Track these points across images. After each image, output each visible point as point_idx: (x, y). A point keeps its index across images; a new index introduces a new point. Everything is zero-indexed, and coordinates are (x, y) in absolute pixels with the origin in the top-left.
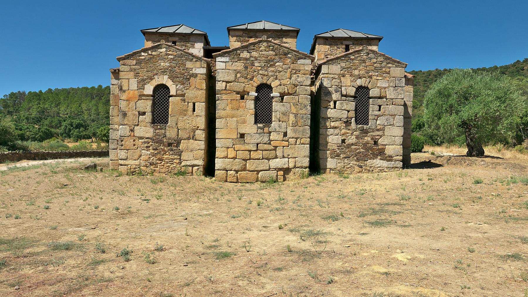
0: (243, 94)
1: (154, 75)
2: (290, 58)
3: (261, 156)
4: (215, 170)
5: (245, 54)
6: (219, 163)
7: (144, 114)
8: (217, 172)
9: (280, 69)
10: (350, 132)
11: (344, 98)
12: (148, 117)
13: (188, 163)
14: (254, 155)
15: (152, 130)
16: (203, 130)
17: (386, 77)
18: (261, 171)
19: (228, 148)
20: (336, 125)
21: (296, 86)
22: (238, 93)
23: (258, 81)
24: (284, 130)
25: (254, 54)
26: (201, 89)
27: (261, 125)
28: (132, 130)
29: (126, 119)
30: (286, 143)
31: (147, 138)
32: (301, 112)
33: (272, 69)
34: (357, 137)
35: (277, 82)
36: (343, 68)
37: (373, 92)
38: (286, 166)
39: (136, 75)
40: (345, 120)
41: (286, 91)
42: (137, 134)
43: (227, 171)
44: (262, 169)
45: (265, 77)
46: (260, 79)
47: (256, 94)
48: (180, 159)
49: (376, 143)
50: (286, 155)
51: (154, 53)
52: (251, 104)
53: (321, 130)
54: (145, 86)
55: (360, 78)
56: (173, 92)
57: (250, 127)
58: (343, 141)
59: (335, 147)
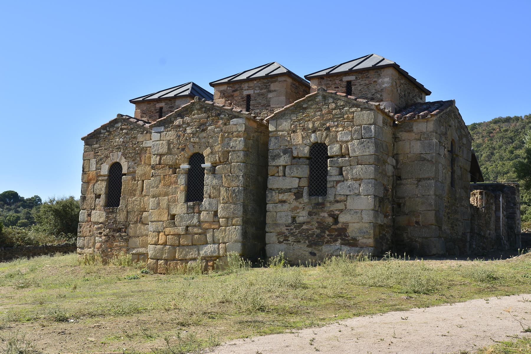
2: (222, 119)
10: (301, 206)
12: (101, 201)
20: (285, 198)
24: (214, 209)
27: (191, 203)
28: (89, 215)
34: (310, 214)
35: (208, 150)
37: (333, 150)
40: (296, 191)
42: (93, 219)
46: (192, 149)
47: (203, 166)
50: (216, 240)
52: (182, 180)
54: (102, 166)
56: (125, 170)
57: (180, 208)
58: (294, 219)
59: (284, 229)
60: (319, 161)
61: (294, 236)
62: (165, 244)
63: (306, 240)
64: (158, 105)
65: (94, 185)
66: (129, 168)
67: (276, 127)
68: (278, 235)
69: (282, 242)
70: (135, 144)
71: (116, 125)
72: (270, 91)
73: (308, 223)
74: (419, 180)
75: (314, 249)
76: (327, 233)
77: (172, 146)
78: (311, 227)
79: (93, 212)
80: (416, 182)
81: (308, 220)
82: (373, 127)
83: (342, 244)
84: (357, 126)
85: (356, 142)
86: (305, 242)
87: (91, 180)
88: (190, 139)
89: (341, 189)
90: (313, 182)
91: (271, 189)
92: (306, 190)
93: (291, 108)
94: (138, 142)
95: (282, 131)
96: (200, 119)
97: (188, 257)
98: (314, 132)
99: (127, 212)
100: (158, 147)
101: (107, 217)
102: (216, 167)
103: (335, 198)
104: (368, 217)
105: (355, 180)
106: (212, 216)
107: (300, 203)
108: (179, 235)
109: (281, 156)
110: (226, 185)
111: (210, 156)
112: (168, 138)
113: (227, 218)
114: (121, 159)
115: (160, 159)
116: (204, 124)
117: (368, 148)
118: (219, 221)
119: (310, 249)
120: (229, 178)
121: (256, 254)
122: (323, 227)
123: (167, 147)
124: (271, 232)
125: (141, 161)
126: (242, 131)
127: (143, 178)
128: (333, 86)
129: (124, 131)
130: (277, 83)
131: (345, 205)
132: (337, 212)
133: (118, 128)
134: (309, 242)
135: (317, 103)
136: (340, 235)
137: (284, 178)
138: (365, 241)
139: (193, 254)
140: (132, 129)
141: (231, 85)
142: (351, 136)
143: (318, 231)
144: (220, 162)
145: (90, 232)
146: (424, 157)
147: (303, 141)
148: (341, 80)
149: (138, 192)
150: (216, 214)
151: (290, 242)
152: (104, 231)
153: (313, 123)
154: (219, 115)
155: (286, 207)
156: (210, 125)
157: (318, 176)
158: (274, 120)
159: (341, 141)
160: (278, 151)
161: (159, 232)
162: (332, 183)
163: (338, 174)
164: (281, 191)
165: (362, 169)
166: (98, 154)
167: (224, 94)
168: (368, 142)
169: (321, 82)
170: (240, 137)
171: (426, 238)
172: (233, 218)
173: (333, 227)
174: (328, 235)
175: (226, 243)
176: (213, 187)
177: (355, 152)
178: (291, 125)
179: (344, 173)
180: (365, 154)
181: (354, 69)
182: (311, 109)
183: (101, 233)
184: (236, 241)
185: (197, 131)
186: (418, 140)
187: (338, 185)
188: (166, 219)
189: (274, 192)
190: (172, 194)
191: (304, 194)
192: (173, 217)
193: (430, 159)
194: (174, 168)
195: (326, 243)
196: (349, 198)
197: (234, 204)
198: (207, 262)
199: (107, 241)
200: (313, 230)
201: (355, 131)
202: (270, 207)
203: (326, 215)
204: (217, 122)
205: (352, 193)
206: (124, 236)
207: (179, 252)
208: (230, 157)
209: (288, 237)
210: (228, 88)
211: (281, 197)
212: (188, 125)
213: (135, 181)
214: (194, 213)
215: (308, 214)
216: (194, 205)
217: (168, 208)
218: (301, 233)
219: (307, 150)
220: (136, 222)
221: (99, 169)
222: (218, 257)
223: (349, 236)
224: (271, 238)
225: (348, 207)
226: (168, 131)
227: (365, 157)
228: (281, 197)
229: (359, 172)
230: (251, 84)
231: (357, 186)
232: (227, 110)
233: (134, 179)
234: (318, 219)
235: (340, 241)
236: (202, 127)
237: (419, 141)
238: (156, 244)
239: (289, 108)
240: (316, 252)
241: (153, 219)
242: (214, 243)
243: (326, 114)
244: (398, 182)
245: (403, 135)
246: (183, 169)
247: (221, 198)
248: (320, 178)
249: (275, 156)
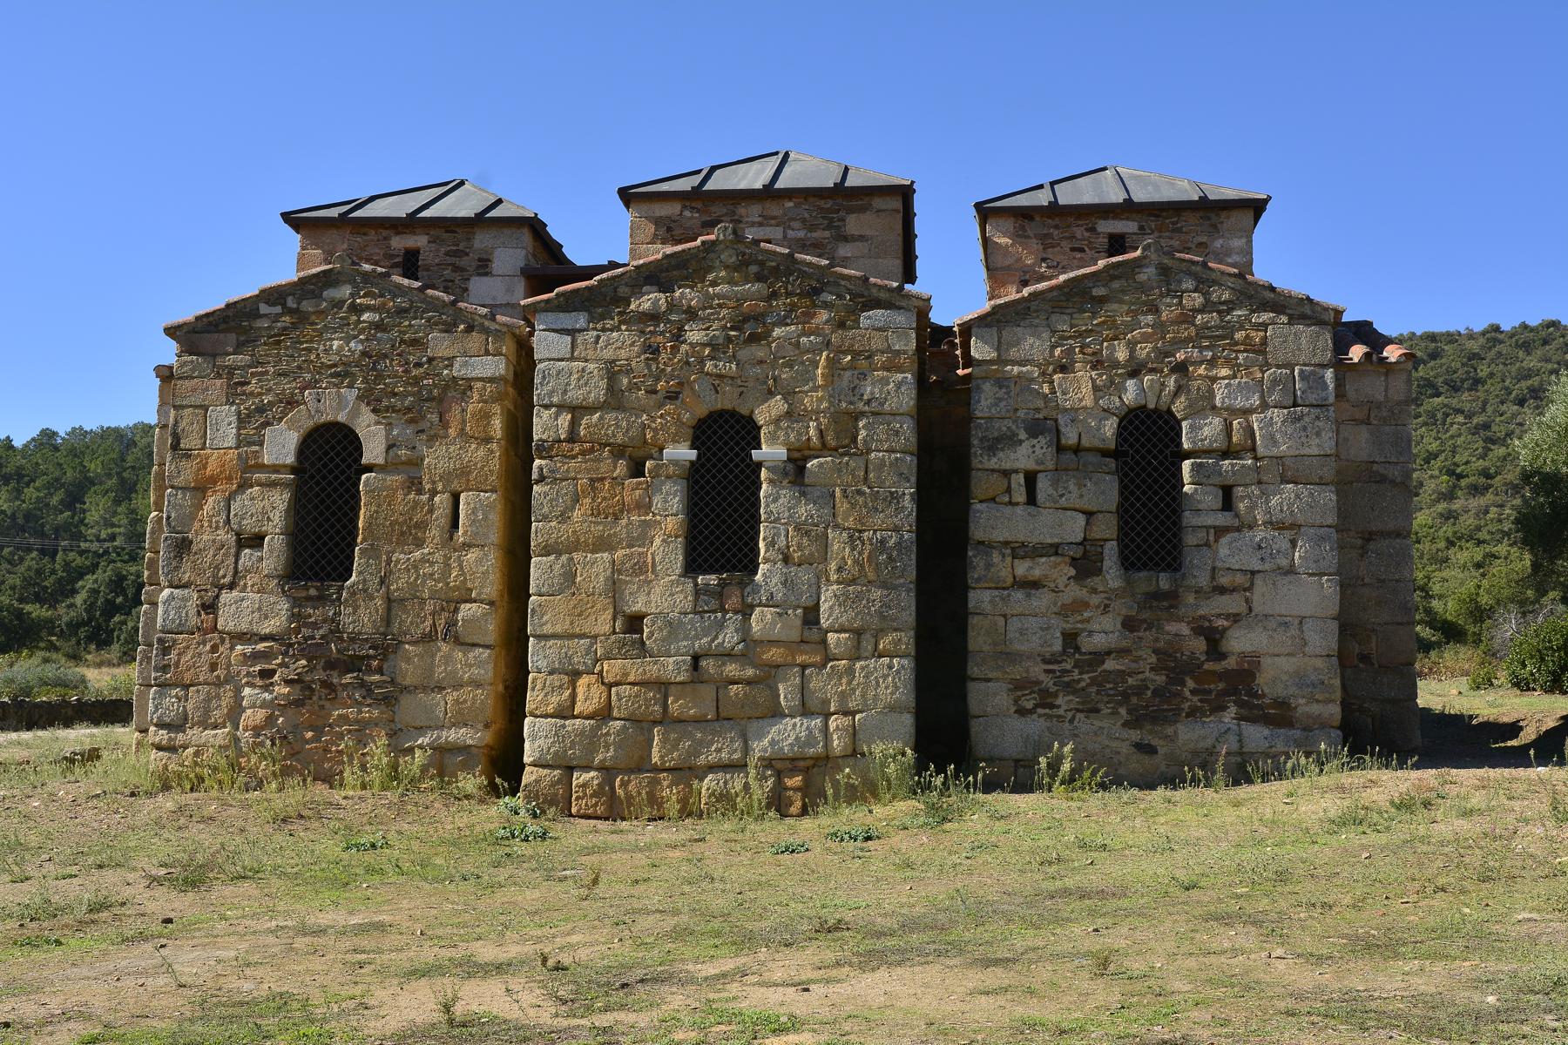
0: (640, 453)
1: (303, 389)
2: (827, 306)
4: (523, 766)
6: (537, 737)
7: (257, 541)
8: (529, 775)
10: (1095, 600)
12: (272, 556)
16: (986, 546)
20: (1037, 573)
22: (619, 452)
24: (805, 600)
27: (713, 579)
28: (210, 607)
29: (186, 565)
34: (1129, 624)
35: (777, 405)
37: (1198, 432)
39: (234, 392)
40: (1079, 552)
43: (570, 769)
47: (692, 454)
50: (813, 704)
52: (669, 505)
53: (971, 594)
56: (373, 452)
57: (665, 593)
58: (1070, 639)
59: (1037, 671)
60: (1150, 463)
61: (1075, 692)
62: (604, 714)
63: (1120, 704)
64: (399, 243)
65: (228, 501)
66: (389, 447)
67: (998, 349)
68: (1017, 688)
69: (1031, 712)
70: (418, 365)
71: (329, 293)
72: (846, 239)
73: (1122, 652)
74: (1369, 537)
75: (1151, 732)
76: (1191, 684)
77: (625, 381)
78: (1134, 665)
79: (226, 597)
80: (1359, 542)
81: (1124, 644)
82: (1329, 374)
83: (1240, 718)
84: (1278, 367)
85: (1277, 415)
86: (1115, 713)
87: (213, 480)
88: (702, 362)
90: (1132, 529)
92: (1111, 551)
93: (1050, 295)
94: (430, 360)
95: (1021, 363)
96: (740, 300)
97: (701, 760)
98: (1134, 373)
99: (389, 600)
100: (563, 380)
101: (293, 617)
102: (806, 459)
103: (1213, 578)
105: (1279, 526)
106: (798, 622)
107: (1094, 591)
108: (662, 686)
109: (1021, 442)
110: (850, 523)
111: (784, 424)
112: (608, 354)
113: (858, 633)
114: (355, 413)
115: (574, 424)
116: (758, 318)
117: (1318, 434)
118: (824, 642)
119: (1135, 735)
120: (861, 500)
121: (948, 744)
122: (1174, 665)
123: (603, 384)
124: (989, 680)
125: (445, 424)
126: (905, 352)
127: (455, 486)
128: (1064, 243)
129: (365, 317)
130: (868, 217)
131: (1247, 600)
132: (1221, 623)
133: (339, 304)
134: (1129, 712)
135: (1143, 288)
136: (1231, 691)
137: (1031, 509)
138: (1315, 709)
139: (723, 748)
140: (401, 312)
141: (699, 205)
142: (1262, 397)
143: (1160, 679)
144: (824, 445)
145: (213, 667)
146: (1382, 471)
147: (1096, 400)
148: (1093, 230)
149: (434, 533)
150: (811, 616)
151: (1061, 712)
152: (283, 665)
153: (1132, 346)
154: (816, 292)
155: (1041, 600)
156: (782, 323)
157: (1150, 511)
158: (989, 326)
159: (1226, 409)
161: (575, 675)
162: (1202, 534)
163: (1220, 505)
164: (1019, 551)
165: (1297, 496)
166: (248, 388)
167: (669, 229)
168: (1318, 418)
169: (1023, 228)
170: (900, 370)
172: (878, 634)
173: (1208, 666)
174: (1193, 692)
175: (853, 714)
176: (797, 529)
177: (1275, 443)
178: (1053, 347)
179: (1241, 507)
180: (1307, 451)
181: (424, 214)
182: (1121, 302)
183: (267, 674)
184: (892, 708)
185: (729, 339)
186: (1362, 422)
188: (607, 628)
190: (630, 546)
191: (1107, 563)
192: (634, 623)
193: (1399, 480)
195: (1188, 716)
196: (1258, 581)
197: (884, 585)
198: (779, 775)
199: (298, 703)
200: (1141, 676)
201: (1275, 382)
202: (980, 598)
203: (1185, 630)
204: (809, 316)
205: (1267, 566)
206: (379, 685)
207: (664, 741)
208: (862, 434)
209: (1055, 695)
210: (687, 213)
211: (1022, 568)
212: (692, 314)
213: (420, 492)
214: (725, 612)
215: (1124, 625)
216: (723, 584)
217: (614, 589)
218: (1100, 685)
219: (1110, 427)
220: (428, 638)
221: (254, 443)
223: (1264, 695)
225: (1257, 608)
226: (604, 330)
227: (1307, 461)
228: (1022, 568)
229: (1290, 505)
230: (774, 209)
231: (1286, 545)
232: (848, 278)
233: (414, 484)
234: (1157, 640)
235: (1233, 709)
236: (750, 327)
237: (1364, 427)
238: (565, 712)
239: (1042, 292)
240: (1154, 742)
241: (547, 629)
242: (805, 711)
243: (1173, 323)
246: (675, 463)
247: (833, 566)
248: (1156, 517)
249: (998, 440)
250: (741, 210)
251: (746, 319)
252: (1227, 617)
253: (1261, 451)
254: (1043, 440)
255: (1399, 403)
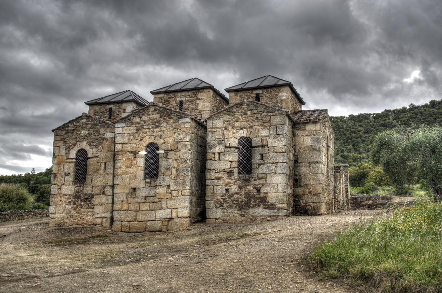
2: (173, 118)
3: (148, 208)
5: (137, 120)
9: (165, 129)
11: (228, 149)
12: (71, 178)
13: (99, 216)
14: (143, 207)
15: (73, 188)
17: (266, 126)
18: (149, 221)
19: (123, 201)
20: (220, 176)
21: (178, 143)
22: (131, 152)
23: (147, 140)
25: (144, 118)
26: (111, 151)
27: (148, 180)
28: (60, 189)
30: (169, 195)
31: (69, 195)
32: (181, 166)
33: (158, 130)
34: (240, 187)
35: (162, 141)
36: (225, 121)
38: (169, 217)
39: (65, 143)
41: (170, 149)
42: (63, 192)
44: (149, 219)
45: (152, 137)
46: (148, 139)
47: (158, 152)
48: (93, 212)
49: (259, 191)
51: (78, 124)
52: (141, 162)
55: (241, 129)
56: (90, 155)
57: (140, 182)
58: (227, 190)
59: (219, 198)
64: (108, 107)
69: (218, 207)
72: (198, 99)
73: (238, 193)
80: (309, 165)
86: (236, 207)
89: (263, 170)
91: (209, 169)
92: (236, 170)
94: (100, 134)
104: (281, 189)
116: (158, 122)
119: (240, 212)
131: (266, 181)
132: (259, 186)
136: (262, 202)
148: (252, 93)
151: (225, 207)
155: (221, 182)
160: (214, 142)
171: (316, 203)
173: (257, 196)
181: (198, 87)
187: (260, 167)
189: (211, 172)
194: (135, 153)
196: (268, 176)
202: (208, 182)
203: (252, 188)
218: (233, 201)
222: (171, 219)
224: (210, 204)
225: (268, 182)
228: (217, 175)
237: (310, 137)
244: (296, 164)
245: (299, 132)
250: (176, 94)
251: (156, 123)
252: (261, 184)
253: (269, 146)
254: (221, 145)
255: (318, 130)
